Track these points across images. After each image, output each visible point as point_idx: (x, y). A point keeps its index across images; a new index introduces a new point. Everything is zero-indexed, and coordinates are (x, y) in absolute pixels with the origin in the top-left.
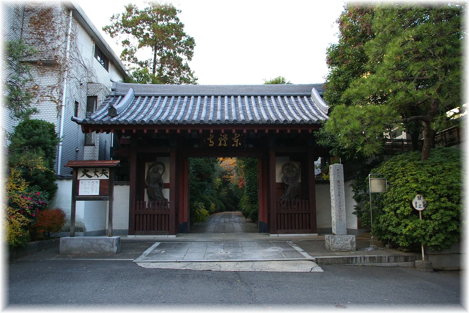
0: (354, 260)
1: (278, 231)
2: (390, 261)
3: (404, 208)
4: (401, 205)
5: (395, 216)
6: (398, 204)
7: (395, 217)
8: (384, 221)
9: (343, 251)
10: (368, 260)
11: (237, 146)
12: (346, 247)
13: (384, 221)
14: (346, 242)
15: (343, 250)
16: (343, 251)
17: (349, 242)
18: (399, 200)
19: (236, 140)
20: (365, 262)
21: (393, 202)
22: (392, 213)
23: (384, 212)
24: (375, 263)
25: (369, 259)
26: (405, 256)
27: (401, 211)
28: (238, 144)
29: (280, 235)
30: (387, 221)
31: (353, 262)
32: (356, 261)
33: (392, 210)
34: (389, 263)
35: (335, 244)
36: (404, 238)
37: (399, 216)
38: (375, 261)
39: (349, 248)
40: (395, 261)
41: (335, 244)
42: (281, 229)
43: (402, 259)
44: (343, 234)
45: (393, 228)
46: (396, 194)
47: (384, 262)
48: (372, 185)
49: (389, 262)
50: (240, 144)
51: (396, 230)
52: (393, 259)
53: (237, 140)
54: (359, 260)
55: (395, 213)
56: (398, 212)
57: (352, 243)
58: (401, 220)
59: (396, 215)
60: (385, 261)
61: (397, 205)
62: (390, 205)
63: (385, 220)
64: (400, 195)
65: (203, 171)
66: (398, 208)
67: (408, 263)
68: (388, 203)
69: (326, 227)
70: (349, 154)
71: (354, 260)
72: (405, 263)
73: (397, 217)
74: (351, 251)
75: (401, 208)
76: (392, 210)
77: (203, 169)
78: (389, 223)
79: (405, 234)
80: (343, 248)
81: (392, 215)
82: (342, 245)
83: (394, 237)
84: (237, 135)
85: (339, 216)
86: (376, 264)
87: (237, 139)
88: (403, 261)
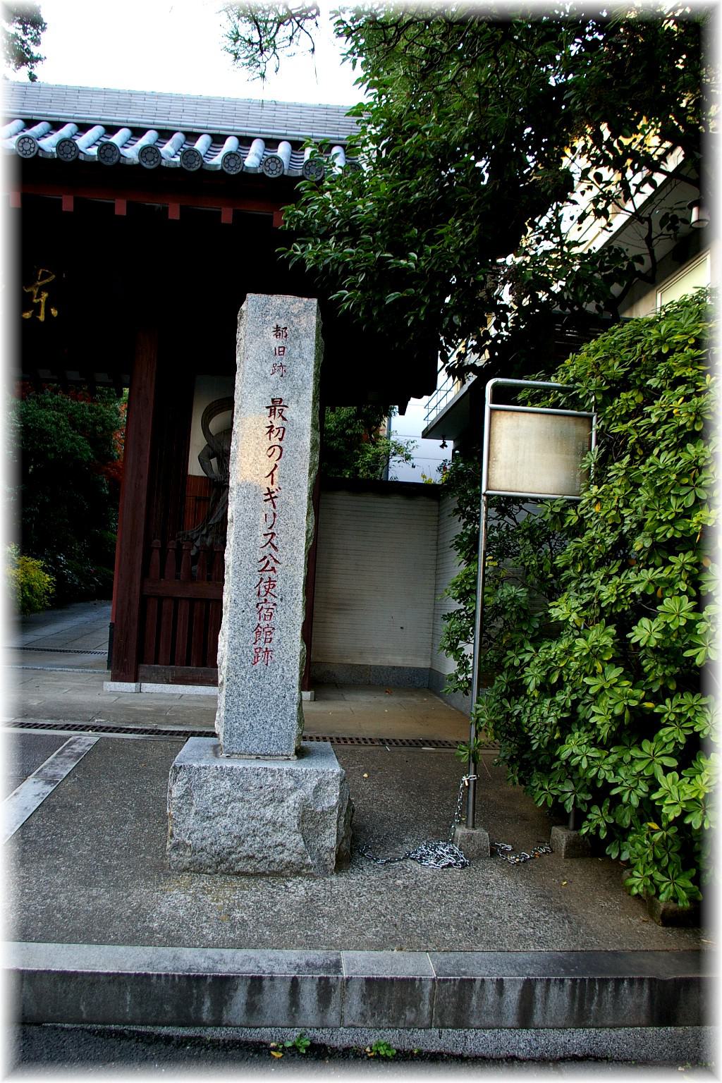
0: (240, 997)
1: (144, 669)
2: (537, 1018)
3: (688, 605)
4: (671, 583)
5: (614, 662)
6: (648, 575)
7: (614, 673)
8: (548, 689)
9: (239, 874)
10: (355, 1005)
11: (42, 318)
12: (269, 842)
13: (548, 689)
14: (269, 813)
15: (240, 866)
16: (239, 874)
17: (288, 810)
18: (655, 545)
19: (39, 296)
20: (332, 1017)
21: (620, 556)
22: (603, 636)
23: (553, 631)
24: (411, 1026)
25: (364, 998)
26: (665, 982)
27: (666, 631)
28: (48, 313)
29: (148, 687)
30: (560, 685)
31: (226, 1017)
32: (252, 1008)
33: (597, 613)
34: (527, 1035)
35: (191, 821)
36: (664, 843)
37: (647, 665)
38: (410, 1015)
39: (286, 856)
40: (580, 1019)
41: (191, 821)
42: (156, 662)
43: (635, 1000)
44: (274, 749)
45: (594, 753)
46: (645, 494)
47: (490, 1020)
48: (537, 491)
49: (525, 1020)
50: (54, 312)
51: (615, 769)
52: (559, 1000)
53: (45, 295)
54: (276, 999)
55: (622, 641)
56: (645, 632)
57: (309, 819)
58: (658, 699)
59: (627, 657)
60: (500, 1013)
61: (641, 580)
62: (598, 575)
63: (554, 679)
64: (667, 507)
65: (53, 450)
66: (646, 606)
67: (680, 1030)
68: (588, 569)
69: (377, 662)
70: (422, 303)
71: (240, 997)
72: (651, 1031)
73: (635, 673)
74: (298, 873)
75: (669, 604)
76: (597, 613)
77: (50, 442)
78: (575, 703)
79: (678, 821)
80: (245, 849)
81: (594, 654)
82: (236, 830)
83: (595, 809)
84: (45, 276)
85: (257, 630)
86: (420, 1034)
87: (42, 289)
88: (643, 1018)
